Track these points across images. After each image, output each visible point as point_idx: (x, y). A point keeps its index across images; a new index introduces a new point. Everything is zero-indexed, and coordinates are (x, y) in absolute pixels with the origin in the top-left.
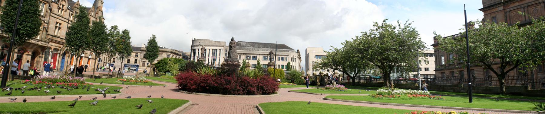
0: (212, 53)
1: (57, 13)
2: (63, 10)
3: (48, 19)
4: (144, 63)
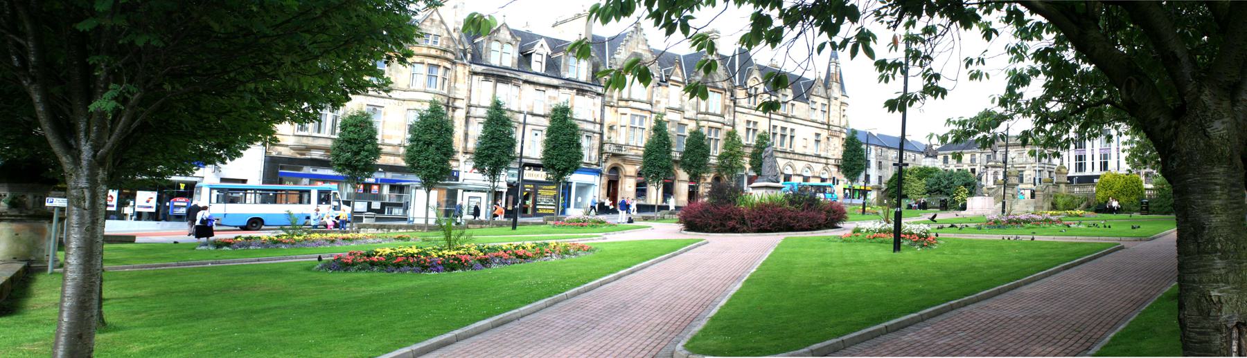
0: (1085, 160)
1: (746, 106)
2: (756, 96)
3: (732, 118)
4: (916, 188)
